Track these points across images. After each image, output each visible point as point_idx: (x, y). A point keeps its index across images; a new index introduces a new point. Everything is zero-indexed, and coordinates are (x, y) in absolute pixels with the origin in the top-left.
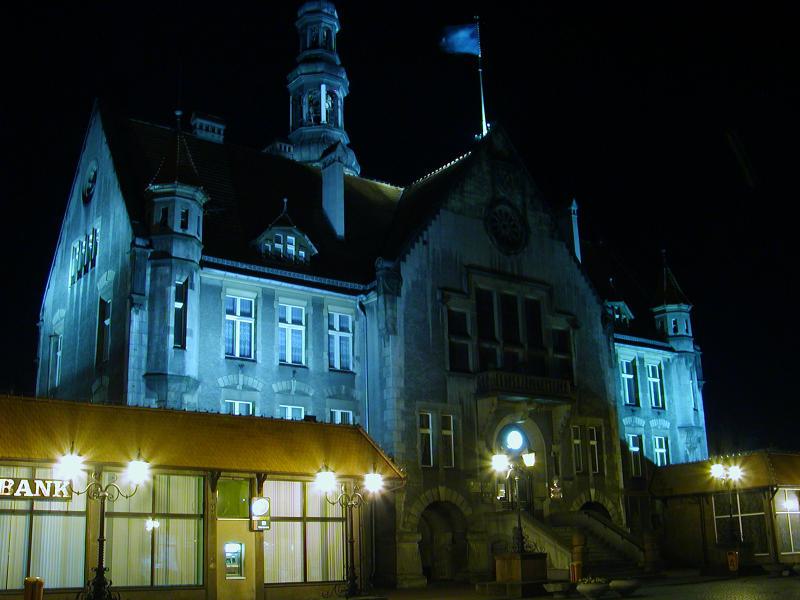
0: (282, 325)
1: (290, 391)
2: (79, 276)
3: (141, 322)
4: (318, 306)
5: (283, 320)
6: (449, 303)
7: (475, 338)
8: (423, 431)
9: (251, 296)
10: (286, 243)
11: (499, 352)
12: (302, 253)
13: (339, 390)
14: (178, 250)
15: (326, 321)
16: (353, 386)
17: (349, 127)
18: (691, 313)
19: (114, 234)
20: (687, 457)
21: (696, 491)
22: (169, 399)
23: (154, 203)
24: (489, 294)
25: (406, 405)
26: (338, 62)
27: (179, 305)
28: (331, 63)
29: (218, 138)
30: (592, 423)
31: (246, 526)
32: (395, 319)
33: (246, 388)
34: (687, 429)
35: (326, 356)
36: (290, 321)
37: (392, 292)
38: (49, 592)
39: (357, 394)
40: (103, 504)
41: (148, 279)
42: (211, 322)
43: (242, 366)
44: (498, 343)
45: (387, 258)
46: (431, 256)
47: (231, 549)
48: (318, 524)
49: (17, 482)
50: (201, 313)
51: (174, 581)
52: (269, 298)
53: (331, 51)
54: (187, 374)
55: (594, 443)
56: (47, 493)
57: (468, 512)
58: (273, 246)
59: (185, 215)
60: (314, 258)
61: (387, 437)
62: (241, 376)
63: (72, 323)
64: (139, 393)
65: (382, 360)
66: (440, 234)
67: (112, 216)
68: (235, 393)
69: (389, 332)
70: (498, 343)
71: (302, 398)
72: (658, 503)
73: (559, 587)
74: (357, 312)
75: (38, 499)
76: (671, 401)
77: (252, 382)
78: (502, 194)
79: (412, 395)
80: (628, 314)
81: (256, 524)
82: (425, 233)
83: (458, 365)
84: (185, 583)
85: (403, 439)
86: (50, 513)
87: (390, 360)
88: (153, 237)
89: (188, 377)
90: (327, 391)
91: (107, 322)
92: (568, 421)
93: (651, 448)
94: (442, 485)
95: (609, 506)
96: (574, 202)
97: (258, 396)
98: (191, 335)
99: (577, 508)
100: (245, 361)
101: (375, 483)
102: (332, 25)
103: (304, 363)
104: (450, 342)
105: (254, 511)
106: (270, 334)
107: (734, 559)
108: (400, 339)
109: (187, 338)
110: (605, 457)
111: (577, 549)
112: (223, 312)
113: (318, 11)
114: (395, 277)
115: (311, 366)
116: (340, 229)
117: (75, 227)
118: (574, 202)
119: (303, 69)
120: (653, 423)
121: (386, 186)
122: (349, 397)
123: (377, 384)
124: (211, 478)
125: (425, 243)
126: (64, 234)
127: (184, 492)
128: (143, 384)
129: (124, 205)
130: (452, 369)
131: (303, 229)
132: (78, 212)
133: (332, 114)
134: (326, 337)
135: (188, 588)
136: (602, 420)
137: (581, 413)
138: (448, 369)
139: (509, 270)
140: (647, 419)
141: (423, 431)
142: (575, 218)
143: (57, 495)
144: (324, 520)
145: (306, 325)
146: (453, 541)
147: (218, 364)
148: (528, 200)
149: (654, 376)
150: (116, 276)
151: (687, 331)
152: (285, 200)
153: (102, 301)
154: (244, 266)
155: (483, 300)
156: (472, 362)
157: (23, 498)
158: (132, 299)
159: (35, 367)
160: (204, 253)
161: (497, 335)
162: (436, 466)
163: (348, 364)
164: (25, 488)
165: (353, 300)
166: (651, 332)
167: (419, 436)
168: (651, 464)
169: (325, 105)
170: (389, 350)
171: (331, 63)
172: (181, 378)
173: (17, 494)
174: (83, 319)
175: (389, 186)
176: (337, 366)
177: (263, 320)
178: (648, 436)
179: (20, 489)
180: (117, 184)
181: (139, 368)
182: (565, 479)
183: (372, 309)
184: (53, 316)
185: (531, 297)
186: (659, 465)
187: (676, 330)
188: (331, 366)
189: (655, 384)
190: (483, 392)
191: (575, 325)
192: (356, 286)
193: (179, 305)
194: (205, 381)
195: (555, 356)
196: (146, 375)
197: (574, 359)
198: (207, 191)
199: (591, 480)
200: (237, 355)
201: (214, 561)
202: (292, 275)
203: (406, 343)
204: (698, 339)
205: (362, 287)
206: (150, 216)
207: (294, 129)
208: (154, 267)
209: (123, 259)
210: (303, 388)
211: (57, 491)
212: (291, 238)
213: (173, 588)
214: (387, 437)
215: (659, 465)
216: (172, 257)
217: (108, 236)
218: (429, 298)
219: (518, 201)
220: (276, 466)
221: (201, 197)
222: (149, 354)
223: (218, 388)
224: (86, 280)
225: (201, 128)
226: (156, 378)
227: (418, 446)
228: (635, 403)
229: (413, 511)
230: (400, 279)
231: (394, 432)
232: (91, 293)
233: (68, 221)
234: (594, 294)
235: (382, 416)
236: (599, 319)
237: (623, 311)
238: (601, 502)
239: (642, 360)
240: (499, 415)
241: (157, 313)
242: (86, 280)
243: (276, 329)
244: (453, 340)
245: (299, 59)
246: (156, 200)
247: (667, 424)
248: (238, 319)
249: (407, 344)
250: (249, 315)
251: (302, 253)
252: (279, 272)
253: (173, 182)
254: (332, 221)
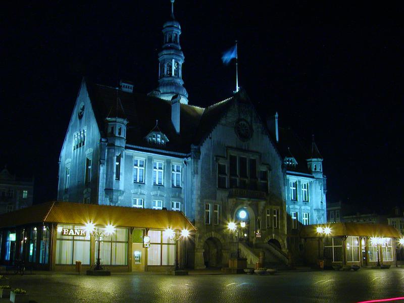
0: (155, 170)
2: (77, 148)
3: (103, 170)
4: (168, 162)
5: (155, 168)
7: (229, 175)
8: (207, 211)
9: (143, 159)
12: (163, 141)
13: (176, 194)
14: (117, 143)
15: (171, 168)
16: (181, 193)
17: (184, 78)
21: (312, 236)
22: (114, 198)
24: (235, 158)
26: (180, 48)
27: (118, 163)
29: (131, 91)
30: (274, 208)
31: (142, 246)
32: (197, 168)
33: (141, 194)
34: (318, 210)
35: (171, 182)
36: (158, 168)
37: (196, 158)
38: (83, 265)
39: (182, 196)
40: (106, 242)
41: (106, 154)
42: (129, 169)
43: (140, 186)
44: (238, 177)
47: (137, 254)
48: (166, 245)
49: (69, 230)
50: (125, 166)
51: (118, 263)
52: (150, 160)
54: (120, 189)
55: (276, 216)
56: (78, 234)
59: (120, 129)
62: (139, 190)
64: (103, 196)
65: (192, 185)
67: (91, 127)
68: (137, 196)
70: (238, 177)
71: (161, 198)
72: (303, 240)
73: (249, 270)
75: (75, 236)
77: (143, 191)
78: (243, 117)
79: (202, 197)
80: (295, 162)
81: (145, 245)
82: (210, 134)
83: (221, 186)
85: (199, 214)
90: (171, 195)
91: (90, 167)
93: (301, 218)
95: (280, 241)
96: (277, 113)
97: (145, 197)
98: (122, 175)
99: (267, 241)
100: (141, 183)
101: (186, 233)
102: (178, 32)
103: (162, 184)
104: (219, 177)
105: (144, 240)
106: (150, 173)
107: (322, 264)
109: (120, 176)
110: (280, 221)
111: (261, 258)
113: (172, 26)
114: (198, 152)
115: (165, 185)
116: (178, 129)
118: (277, 113)
119: (165, 52)
120: (303, 207)
121: (198, 108)
122: (179, 197)
123: (190, 193)
124: (131, 230)
125: (210, 138)
126: (70, 128)
127: (122, 234)
128: (104, 193)
132: (76, 120)
133: (177, 71)
134: (171, 174)
137: (271, 204)
138: (217, 187)
140: (300, 206)
141: (207, 211)
142: (276, 120)
143: (81, 234)
144: (169, 244)
145: (164, 170)
146: (217, 252)
148: (253, 119)
149: (305, 188)
150: (94, 151)
151: (320, 170)
153: (88, 160)
154: (141, 148)
155: (233, 160)
156: (227, 185)
157: (71, 235)
158: (100, 162)
159: (58, 179)
160: (127, 143)
161: (237, 173)
162: (211, 224)
164: (72, 232)
165: (181, 160)
166: (304, 169)
169: (174, 68)
170: (195, 180)
171: (177, 49)
172: (118, 191)
173: (70, 234)
175: (199, 108)
176: (175, 185)
177: (148, 168)
178: (300, 213)
179: (70, 233)
180: (93, 115)
181: (103, 187)
183: (189, 164)
184: (65, 160)
186: (305, 224)
187: (315, 169)
189: (305, 191)
191: (270, 170)
192: (184, 155)
193: (118, 163)
194: (127, 191)
196: (106, 189)
197: (269, 183)
199: (273, 230)
200: (138, 181)
206: (107, 129)
207: (161, 78)
208: (108, 149)
210: (163, 194)
212: (159, 136)
215: (305, 224)
221: (126, 122)
225: (124, 86)
226: (109, 191)
227: (205, 216)
230: (200, 152)
231: (196, 212)
233: (71, 124)
235: (191, 205)
236: (280, 166)
237: (294, 162)
238: (277, 239)
239: (299, 182)
240: (236, 205)
241: (110, 165)
242: (80, 150)
244: (220, 176)
245: (164, 46)
246: (109, 123)
247: (309, 208)
248: (138, 168)
249: (202, 178)
250: (143, 166)
254: (175, 127)
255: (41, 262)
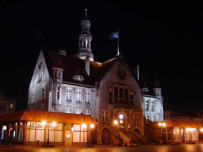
0: (77, 94)
2: (38, 83)
3: (51, 94)
4: (84, 90)
5: (77, 93)
7: (114, 97)
8: (103, 115)
9: (71, 89)
10: (78, 78)
11: (119, 99)
12: (81, 80)
13: (87, 106)
14: (58, 81)
15: (85, 93)
16: (90, 105)
25: (100, 110)
26: (90, 33)
27: (58, 91)
28: (88, 34)
29: (65, 54)
30: (137, 113)
31: (70, 132)
33: (70, 106)
34: (159, 114)
37: (98, 88)
38: (40, 142)
39: (91, 107)
41: (53, 86)
42: (64, 94)
43: (69, 102)
45: (97, 82)
46: (106, 81)
47: (68, 136)
49: (34, 124)
51: (58, 141)
53: (88, 31)
54: (59, 104)
55: (138, 117)
56: (38, 126)
57: (111, 130)
59: (60, 74)
60: (83, 81)
62: (69, 104)
65: (96, 102)
72: (151, 129)
73: (124, 145)
74: (91, 92)
76: (156, 108)
77: (71, 105)
78: (121, 68)
79: (101, 108)
80: (148, 90)
82: (105, 76)
83: (110, 102)
84: (60, 142)
86: (39, 129)
87: (97, 101)
89: (60, 104)
90: (85, 107)
91: (44, 93)
93: (151, 118)
94: (106, 125)
95: (140, 130)
96: (138, 66)
99: (133, 130)
100: (69, 101)
101: (92, 126)
106: (75, 96)
107: (161, 141)
108: (99, 97)
112: (66, 91)
114: (99, 85)
115: (82, 102)
116: (89, 74)
117: (37, 72)
118: (138, 66)
119: (82, 35)
120: (151, 113)
123: (95, 106)
124: (65, 124)
125: (105, 78)
126: (34, 73)
128: (51, 105)
129: (48, 71)
130: (109, 103)
133: (88, 45)
135: (60, 142)
136: (139, 113)
138: (108, 103)
139: (122, 83)
140: (150, 112)
142: (138, 69)
144: (84, 131)
147: (65, 102)
148: (126, 68)
149: (152, 103)
152: (86, 10)
154: (70, 83)
155: (116, 89)
156: (113, 101)
157: (34, 127)
160: (63, 81)
162: (105, 122)
163: (89, 101)
166: (152, 94)
168: (150, 121)
169: (87, 43)
170: (97, 99)
171: (88, 34)
172: (58, 104)
173: (34, 126)
175: (99, 63)
176: (87, 102)
182: (131, 124)
185: (126, 88)
186: (152, 121)
187: (158, 94)
188: (86, 102)
190: (115, 107)
191: (135, 94)
192: (91, 86)
193: (58, 91)
195: (130, 100)
196: (52, 104)
197: (134, 101)
198: (63, 69)
200: (68, 100)
201: (65, 138)
202: (79, 84)
204: (162, 95)
208: (53, 83)
209: (48, 82)
211: (40, 126)
212: (79, 77)
213: (58, 142)
215: (152, 121)
217: (44, 76)
218: (105, 89)
219: (124, 69)
220: (76, 123)
221: (62, 70)
222: (52, 100)
223: (65, 106)
224: (39, 84)
226: (54, 104)
228: (148, 109)
229: (101, 130)
230: (100, 85)
232: (41, 86)
233: (35, 71)
236: (140, 92)
239: (150, 100)
240: (118, 112)
241: (54, 92)
242: (39, 84)
243: (76, 95)
245: (81, 32)
247: (155, 113)
248: (69, 93)
249: (101, 98)
252: (77, 84)
253: (57, 68)
255: (19, 140)
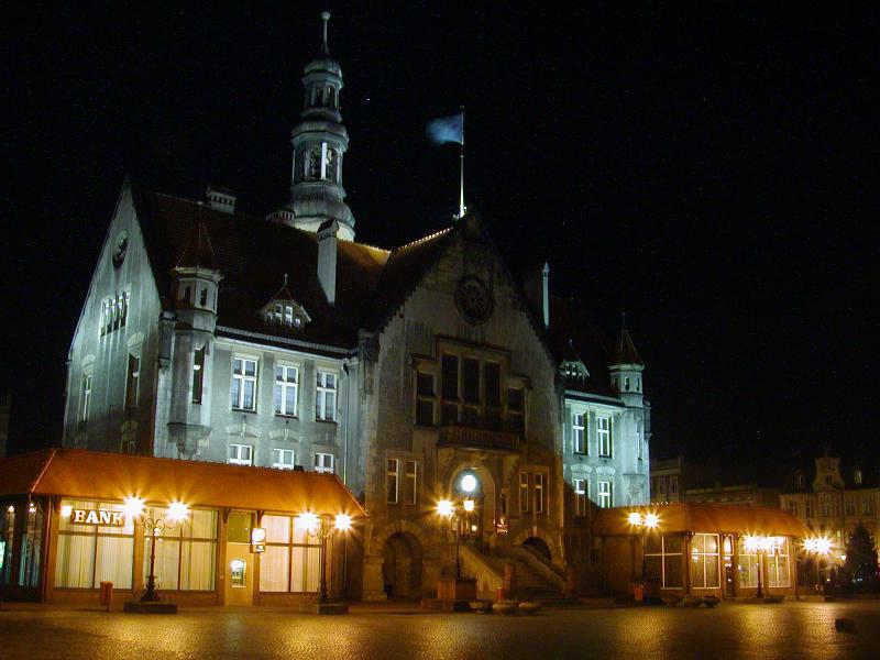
0: (279, 383)
1: (283, 438)
2: (109, 331)
3: (166, 381)
4: (309, 367)
5: (280, 379)
6: (419, 367)
7: (440, 397)
9: (254, 359)
12: (298, 321)
13: (323, 437)
14: (198, 323)
16: (334, 433)
17: (346, 185)
18: (644, 374)
19: (143, 302)
20: (629, 500)
23: (178, 282)
26: (340, 119)
27: (197, 368)
28: (332, 121)
29: (230, 209)
30: (540, 470)
31: (248, 549)
32: (372, 381)
33: (248, 435)
34: (631, 476)
36: (285, 379)
37: (370, 358)
39: (338, 441)
42: (222, 382)
43: (245, 417)
47: (236, 565)
49: (88, 512)
52: (269, 361)
53: (334, 109)
55: (540, 487)
56: (108, 521)
57: (424, 542)
58: (274, 316)
59: (204, 293)
60: (307, 325)
61: (360, 478)
62: (244, 425)
63: (102, 369)
66: (416, 307)
68: (239, 439)
69: (366, 392)
72: (598, 540)
73: (480, 605)
74: (341, 371)
77: (253, 430)
79: (382, 445)
80: (585, 372)
83: (423, 420)
86: (109, 535)
87: (366, 416)
88: (179, 311)
90: (313, 438)
91: (136, 375)
92: (516, 470)
95: (549, 541)
97: (257, 442)
98: (206, 393)
101: (344, 523)
105: (254, 538)
106: (269, 390)
107: (639, 592)
108: (376, 397)
112: (232, 371)
113: (324, 71)
114: (374, 346)
115: (301, 417)
116: (331, 295)
119: (306, 127)
120: (599, 470)
123: (355, 434)
124: (224, 514)
125: (401, 316)
126: (94, 288)
127: (205, 523)
128: (166, 431)
131: (299, 302)
132: (107, 274)
133: (331, 169)
134: (315, 393)
135: (204, 592)
137: (529, 461)
139: (473, 338)
140: (594, 466)
143: (114, 522)
144: (306, 546)
146: (412, 565)
148: (495, 276)
149: (604, 428)
153: (131, 356)
154: (250, 334)
155: (449, 364)
156: (436, 419)
157: (91, 524)
158: (159, 362)
161: (459, 395)
162: (400, 504)
163: (332, 414)
165: (339, 363)
166: (603, 388)
167: (386, 478)
169: (325, 162)
170: (365, 407)
171: (332, 121)
172: (197, 427)
174: (113, 367)
175: (377, 249)
176: (323, 417)
178: (593, 481)
179: (89, 518)
181: (164, 418)
184: (82, 358)
186: (603, 506)
187: (627, 387)
188: (318, 416)
189: (605, 435)
191: (530, 387)
192: (343, 351)
193: (197, 368)
194: (215, 428)
195: (511, 412)
196: (169, 424)
198: (221, 273)
200: (242, 407)
202: (289, 341)
203: (380, 401)
204: (647, 395)
205: (346, 351)
207: (296, 182)
212: (290, 308)
214: (360, 478)
215: (603, 506)
216: (193, 329)
217: (138, 303)
219: (486, 277)
221: (217, 277)
223: (227, 434)
226: (177, 427)
228: (584, 452)
230: (377, 347)
233: (97, 278)
234: (549, 358)
236: (552, 380)
239: (593, 414)
240: (454, 464)
244: (421, 398)
245: (304, 115)
247: (613, 471)
248: (243, 378)
249: (381, 401)
251: (298, 321)
254: (324, 286)
